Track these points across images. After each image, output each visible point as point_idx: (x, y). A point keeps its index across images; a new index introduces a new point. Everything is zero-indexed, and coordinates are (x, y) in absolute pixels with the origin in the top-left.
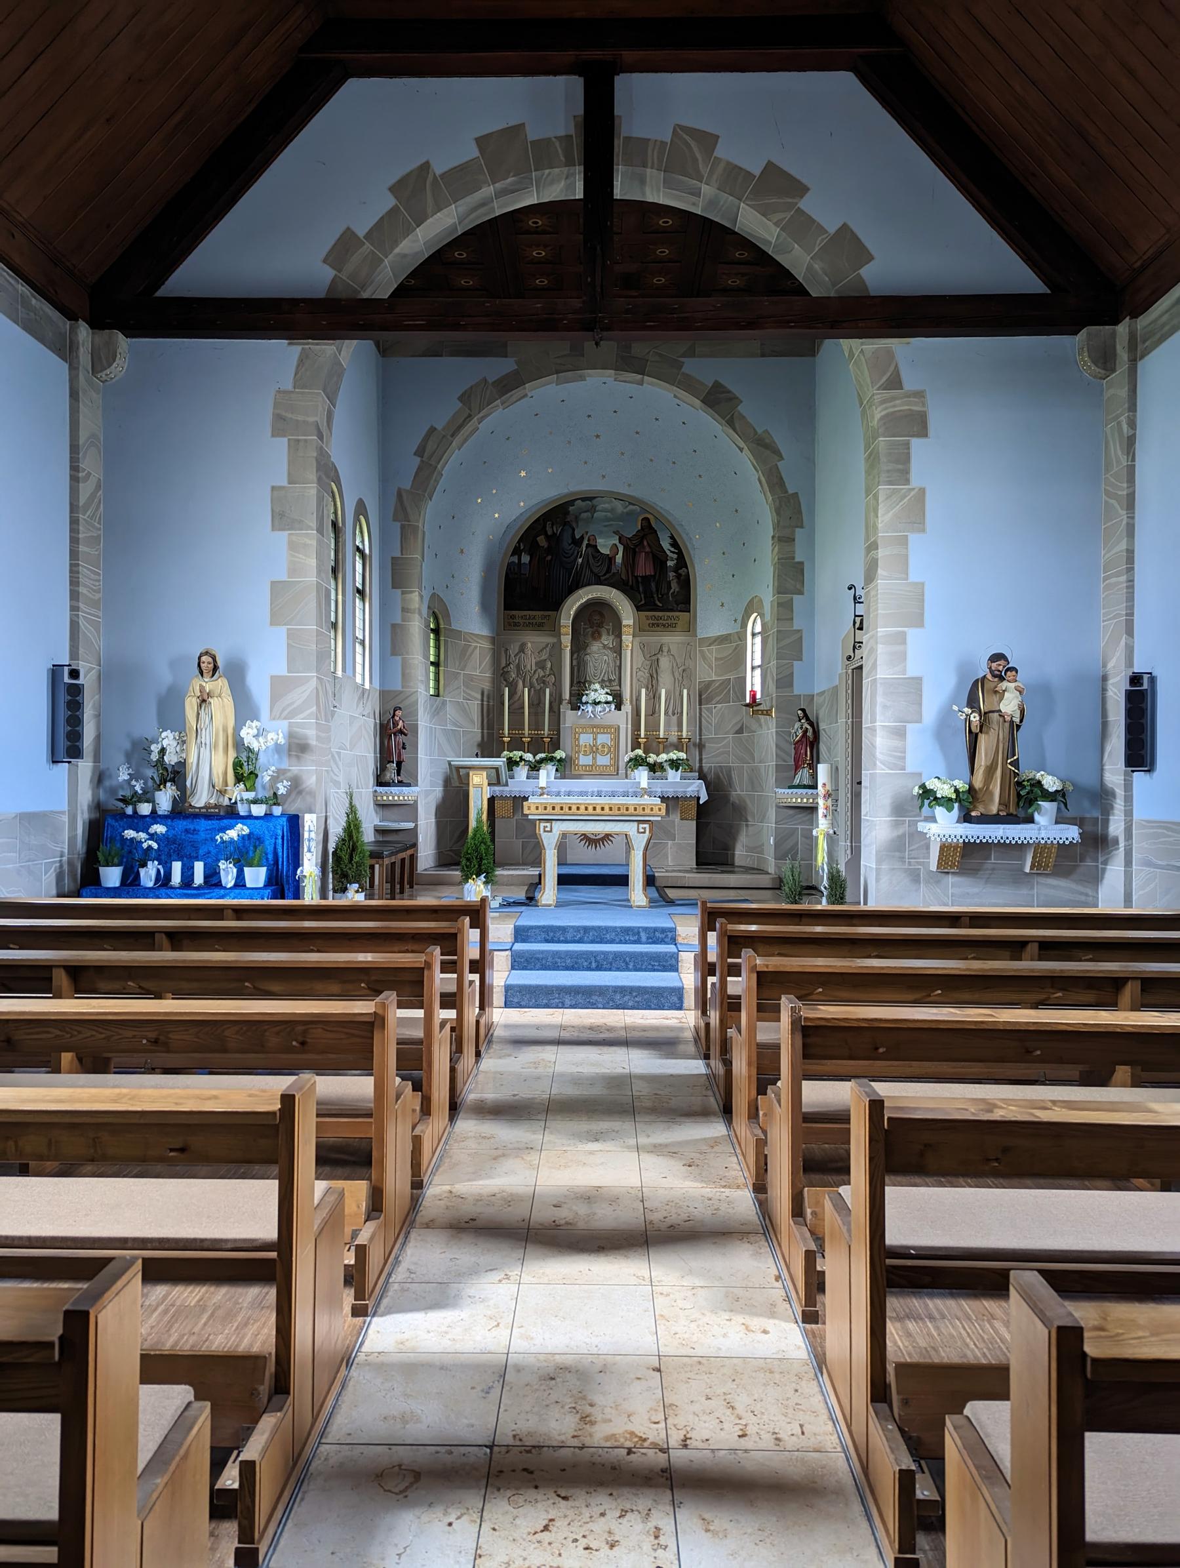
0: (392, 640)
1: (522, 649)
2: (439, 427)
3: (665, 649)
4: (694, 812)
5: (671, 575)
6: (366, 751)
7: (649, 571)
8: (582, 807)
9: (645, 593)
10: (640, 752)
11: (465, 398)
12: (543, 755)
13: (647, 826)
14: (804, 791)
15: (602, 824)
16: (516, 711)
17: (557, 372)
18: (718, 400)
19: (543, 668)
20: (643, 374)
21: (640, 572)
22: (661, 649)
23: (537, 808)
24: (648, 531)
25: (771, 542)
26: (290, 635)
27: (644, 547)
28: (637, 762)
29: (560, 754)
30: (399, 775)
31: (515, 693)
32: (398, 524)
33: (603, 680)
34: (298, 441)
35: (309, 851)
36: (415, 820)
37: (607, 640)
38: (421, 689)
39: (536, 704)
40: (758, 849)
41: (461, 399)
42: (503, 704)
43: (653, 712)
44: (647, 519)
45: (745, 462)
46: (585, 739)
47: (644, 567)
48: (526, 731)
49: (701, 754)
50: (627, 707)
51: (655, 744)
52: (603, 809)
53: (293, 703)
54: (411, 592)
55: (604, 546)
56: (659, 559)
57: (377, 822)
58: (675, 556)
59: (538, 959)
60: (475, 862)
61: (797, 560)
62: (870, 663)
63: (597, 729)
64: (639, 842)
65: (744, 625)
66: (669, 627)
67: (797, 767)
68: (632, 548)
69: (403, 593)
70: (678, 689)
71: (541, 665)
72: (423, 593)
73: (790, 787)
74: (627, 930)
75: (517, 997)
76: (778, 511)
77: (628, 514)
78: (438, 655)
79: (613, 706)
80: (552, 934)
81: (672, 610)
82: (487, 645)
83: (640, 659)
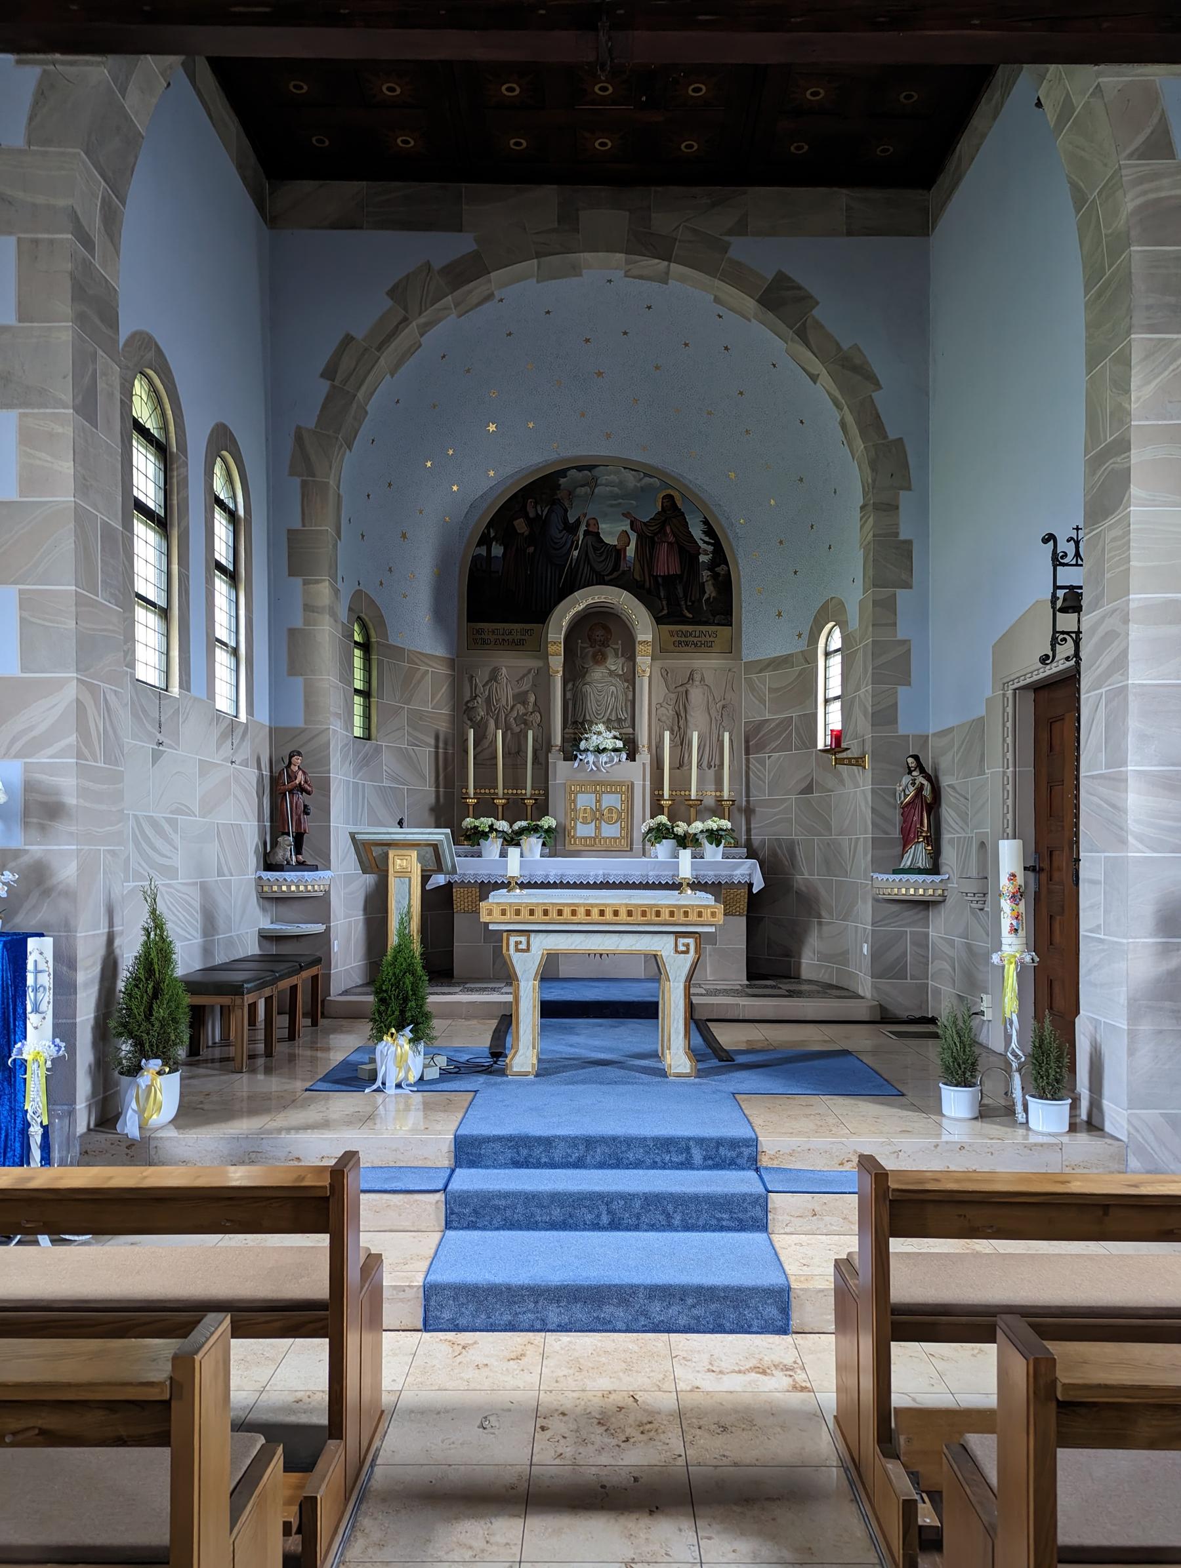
0: (289, 652)
1: (494, 676)
2: (359, 335)
3: (697, 677)
4: (743, 905)
5: (706, 574)
6: (242, 818)
8: (581, 911)
10: (663, 819)
11: (397, 293)
12: (524, 823)
13: (691, 941)
14: (920, 878)
15: (615, 937)
16: (486, 763)
17: (538, 255)
18: (782, 300)
19: (525, 703)
20: (670, 260)
22: (691, 678)
23: (504, 913)
24: (672, 513)
25: (857, 514)
26: (25, 602)
27: (665, 534)
28: (660, 833)
29: (548, 822)
30: (298, 851)
31: (484, 736)
32: (298, 480)
34: (36, 242)
35: (36, 1010)
36: (326, 919)
37: (614, 664)
38: (336, 727)
39: (514, 753)
40: (842, 957)
41: (391, 293)
42: (466, 752)
43: (680, 764)
44: (670, 497)
45: (820, 400)
46: (585, 801)
47: (666, 564)
49: (748, 823)
50: (644, 757)
52: (616, 913)
53: (31, 728)
54: (317, 582)
55: (611, 533)
56: (687, 552)
57: (266, 924)
58: (710, 548)
59: (497, 1208)
60: (394, 1005)
61: (902, 537)
62: (1105, 660)
63: (601, 786)
64: (678, 967)
65: (813, 640)
66: (701, 646)
67: (906, 842)
68: (648, 539)
69: (305, 583)
70: (715, 732)
71: (521, 698)
72: (340, 585)
73: (895, 872)
74: (666, 1144)
75: (452, 1308)
76: (874, 465)
77: (642, 489)
78: (368, 681)
79: (624, 756)
80: (525, 1151)
82: (443, 670)
83: (661, 690)
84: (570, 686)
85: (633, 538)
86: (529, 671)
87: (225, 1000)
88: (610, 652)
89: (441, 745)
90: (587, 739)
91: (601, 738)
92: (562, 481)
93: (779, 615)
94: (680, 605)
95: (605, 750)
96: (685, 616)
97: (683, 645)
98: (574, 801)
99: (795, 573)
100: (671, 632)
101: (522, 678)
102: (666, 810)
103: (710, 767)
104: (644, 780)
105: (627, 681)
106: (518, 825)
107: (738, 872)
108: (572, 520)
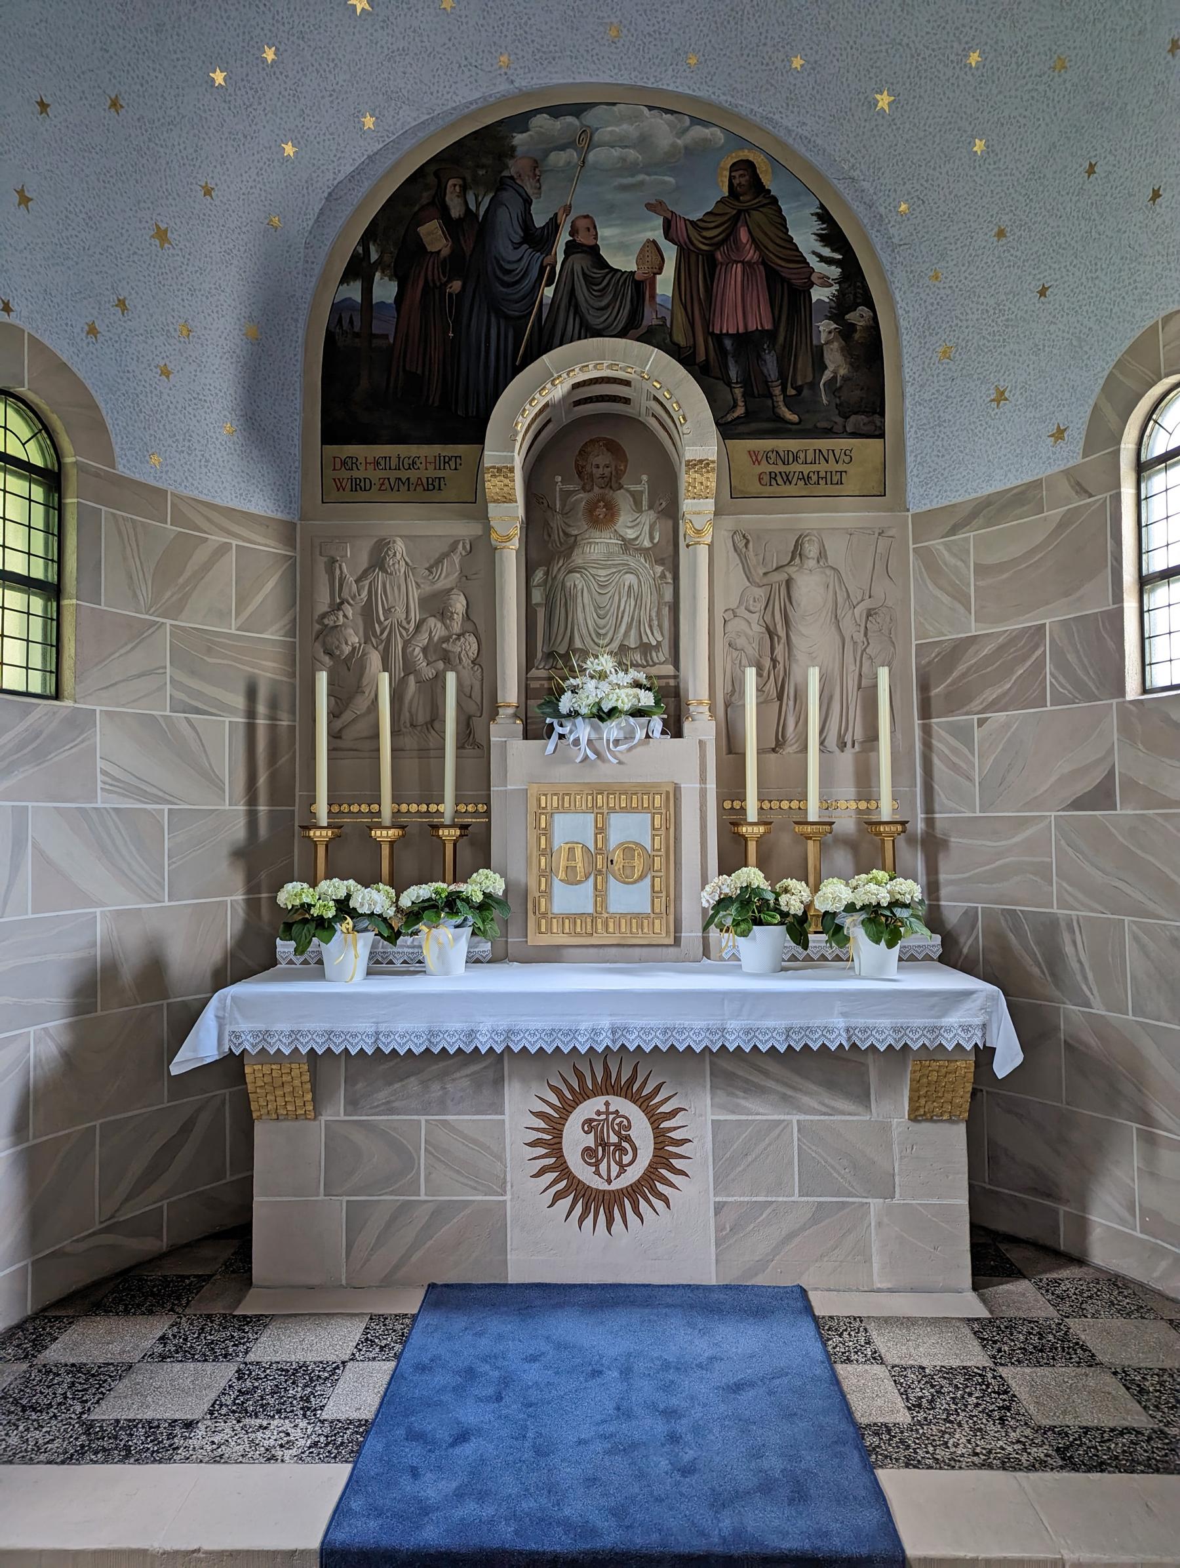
1: (379, 560)
3: (811, 550)
5: (824, 328)
7: (759, 318)
9: (746, 383)
10: (751, 875)
16: (353, 745)
19: (443, 614)
21: (730, 323)
22: (797, 552)
24: (750, 194)
27: (738, 247)
28: (750, 910)
29: (484, 883)
33: (623, 649)
37: (635, 524)
44: (748, 166)
46: (571, 828)
47: (742, 308)
48: (387, 807)
50: (702, 727)
51: (785, 840)
55: (622, 247)
56: (786, 285)
58: (834, 272)
63: (606, 798)
66: (824, 483)
68: (701, 262)
71: (436, 605)
77: (689, 151)
79: (657, 724)
81: (828, 433)
82: (267, 546)
83: (734, 580)
84: (539, 575)
85: (671, 254)
86: (453, 548)
87: (592, 756)
88: (623, 500)
91: (605, 686)
92: (519, 139)
93: (1000, 397)
95: (613, 712)
97: (780, 480)
98: (547, 832)
99: (1043, 292)
100: (755, 457)
101: (439, 561)
102: (752, 847)
103: (842, 746)
104: (703, 780)
105: (660, 562)
107: (952, 1020)
108: (539, 221)
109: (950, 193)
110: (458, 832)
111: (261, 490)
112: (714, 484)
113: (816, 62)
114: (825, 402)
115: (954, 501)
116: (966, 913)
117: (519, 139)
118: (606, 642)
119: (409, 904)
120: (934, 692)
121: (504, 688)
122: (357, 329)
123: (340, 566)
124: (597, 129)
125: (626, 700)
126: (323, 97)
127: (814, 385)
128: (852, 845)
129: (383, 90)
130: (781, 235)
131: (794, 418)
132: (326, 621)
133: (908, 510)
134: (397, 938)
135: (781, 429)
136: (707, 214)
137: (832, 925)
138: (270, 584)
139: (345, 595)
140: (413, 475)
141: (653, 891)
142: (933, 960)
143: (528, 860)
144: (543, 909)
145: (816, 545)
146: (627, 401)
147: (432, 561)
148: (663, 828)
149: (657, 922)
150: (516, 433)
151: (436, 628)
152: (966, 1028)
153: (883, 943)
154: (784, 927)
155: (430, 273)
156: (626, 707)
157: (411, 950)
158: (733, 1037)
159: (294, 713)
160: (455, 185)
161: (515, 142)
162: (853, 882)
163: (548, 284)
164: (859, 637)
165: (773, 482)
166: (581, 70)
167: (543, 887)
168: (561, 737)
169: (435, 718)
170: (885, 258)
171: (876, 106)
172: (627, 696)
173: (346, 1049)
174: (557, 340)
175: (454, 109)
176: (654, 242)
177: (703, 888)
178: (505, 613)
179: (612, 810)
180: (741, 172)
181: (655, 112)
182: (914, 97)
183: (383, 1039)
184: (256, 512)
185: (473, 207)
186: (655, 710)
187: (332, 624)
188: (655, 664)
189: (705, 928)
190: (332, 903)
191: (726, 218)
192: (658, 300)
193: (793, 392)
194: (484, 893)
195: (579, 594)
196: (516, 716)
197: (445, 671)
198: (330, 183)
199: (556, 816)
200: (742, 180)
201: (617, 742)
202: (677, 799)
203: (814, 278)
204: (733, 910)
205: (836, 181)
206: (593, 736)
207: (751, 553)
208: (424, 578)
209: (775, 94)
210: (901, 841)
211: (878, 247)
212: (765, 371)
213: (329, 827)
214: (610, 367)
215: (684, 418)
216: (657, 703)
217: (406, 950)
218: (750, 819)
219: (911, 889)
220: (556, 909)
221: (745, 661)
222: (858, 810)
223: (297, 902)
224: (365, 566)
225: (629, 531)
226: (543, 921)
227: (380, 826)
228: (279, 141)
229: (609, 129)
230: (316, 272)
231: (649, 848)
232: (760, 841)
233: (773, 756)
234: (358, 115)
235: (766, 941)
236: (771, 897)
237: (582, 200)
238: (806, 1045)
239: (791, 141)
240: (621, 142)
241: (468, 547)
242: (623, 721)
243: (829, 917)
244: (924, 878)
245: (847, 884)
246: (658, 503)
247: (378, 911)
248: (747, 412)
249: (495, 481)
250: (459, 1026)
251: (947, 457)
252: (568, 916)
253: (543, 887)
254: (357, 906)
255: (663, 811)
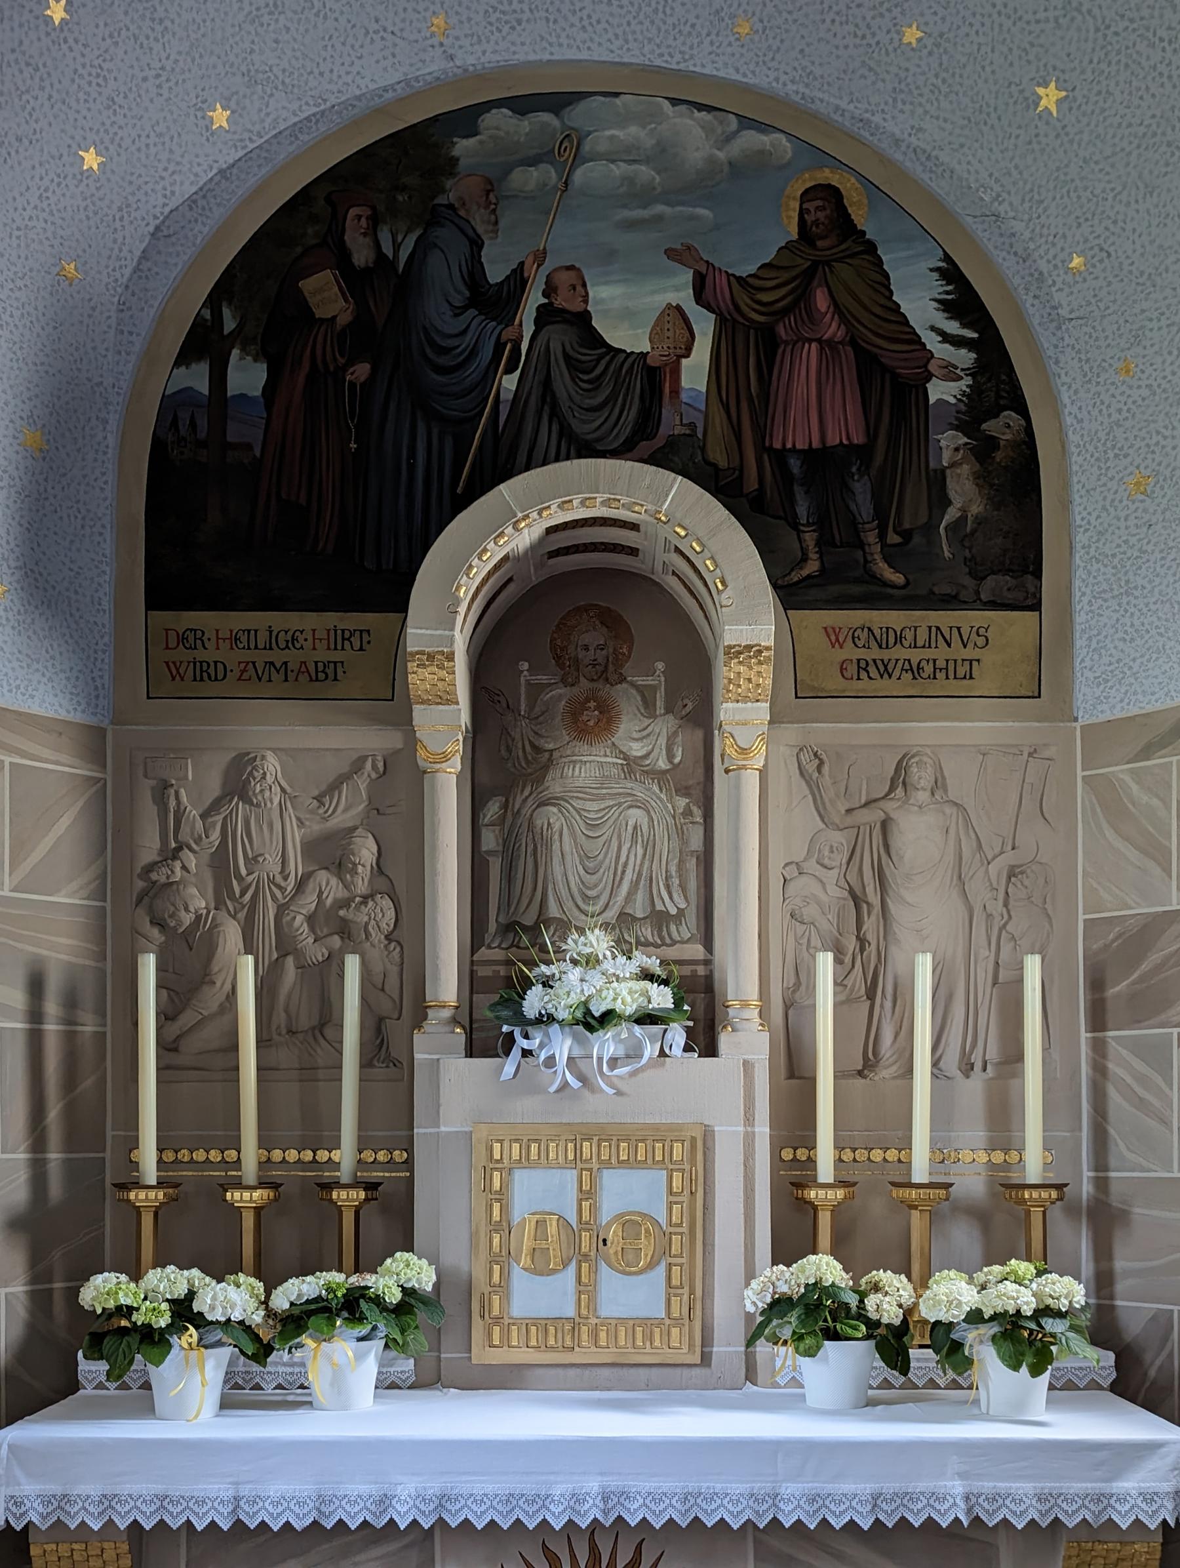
1: (239, 783)
3: (922, 776)
7: (844, 425)
9: (822, 523)
16: (195, 1060)
19: (341, 866)
22: (900, 779)
24: (835, 235)
28: (819, 1318)
33: (625, 919)
37: (645, 736)
39: (295, 1032)
43: (871, 1058)
44: (831, 195)
47: (816, 409)
50: (748, 1041)
51: (877, 1207)
55: (628, 315)
56: (886, 372)
58: (965, 358)
63: (599, 1146)
66: (942, 677)
68: (755, 328)
71: (329, 852)
77: (736, 169)
79: (677, 1035)
81: (950, 602)
82: (60, 764)
83: (799, 822)
84: (493, 809)
85: (704, 326)
86: (357, 766)
88: (626, 701)
89: (52, 1007)
90: (547, 983)
91: (596, 979)
92: (463, 147)
94: (861, 545)
95: (607, 1018)
96: (886, 584)
97: (874, 672)
98: (503, 1196)
101: (334, 787)
102: (825, 1220)
103: (967, 1068)
104: (749, 1119)
105: (684, 791)
106: (296, 1290)
107: (1129, 1485)
108: (496, 273)
109: (1152, 242)
110: (362, 1195)
111: (50, 680)
112: (769, 682)
113: (941, 35)
114: (947, 554)
115: (1149, 709)
116: (1154, 1318)
117: (463, 147)
118: (598, 908)
119: (287, 1306)
120: (1111, 992)
121: (436, 978)
122: (202, 435)
123: (177, 793)
124: (589, 133)
125: (629, 999)
126: (145, 79)
127: (930, 528)
128: (981, 1216)
129: (244, 68)
130: (883, 301)
131: (899, 579)
132: (154, 876)
133: (1076, 719)
134: (267, 1355)
135: (878, 596)
136: (763, 266)
137: (947, 1343)
138: (65, 822)
139: (185, 835)
140: (293, 657)
141: (671, 1192)
142: (1101, 1388)
143: (473, 1237)
144: (496, 1312)
145: (930, 770)
146: (633, 552)
147: (324, 787)
148: (686, 1192)
149: (675, 1332)
150: (457, 601)
151: (330, 887)
152: (1149, 1497)
153: (1024, 1369)
154: (871, 1344)
155: (319, 347)
156: (629, 1010)
157: (289, 1370)
158: (791, 1507)
159: (104, 1016)
160: (359, 217)
161: (456, 151)
162: (980, 1277)
163: (509, 370)
164: (997, 908)
165: (863, 675)
166: (565, 41)
167: (496, 1278)
168: (526, 1053)
169: (327, 1019)
170: (1046, 340)
171: (1037, 105)
172: (631, 992)
173: (188, 1522)
174: (522, 458)
175: (358, 98)
176: (679, 308)
177: (747, 1284)
178: (439, 866)
179: (607, 1164)
180: (819, 203)
181: (683, 108)
182: (1099, 93)
183: (246, 1508)
184: (41, 712)
185: (388, 250)
186: (674, 1015)
187: (163, 879)
188: (674, 943)
189: (750, 1342)
190: (165, 1306)
191: (794, 273)
192: (684, 397)
193: (897, 539)
194: (404, 1290)
195: (556, 837)
196: (454, 1021)
197: (342, 952)
198: (158, 210)
199: (518, 1175)
200: (819, 214)
201: (614, 1062)
202: (708, 1151)
203: (932, 367)
204: (793, 1318)
205: (969, 219)
206: (576, 1052)
207: (826, 780)
208: (312, 812)
209: (874, 83)
210: (1056, 1212)
211: (1036, 322)
212: (853, 507)
213: (160, 1184)
214: (606, 503)
215: (723, 583)
216: (678, 1003)
217: (281, 1369)
218: (822, 1179)
219: (1069, 1291)
220: (516, 1311)
221: (816, 942)
222: (990, 1164)
223: (111, 1304)
224: (217, 792)
225: (635, 746)
226: (497, 1329)
227: (239, 1185)
228: (74, 146)
229: (608, 133)
230: (137, 348)
231: (663, 1221)
232: (837, 1210)
233: (860, 1082)
234: (202, 107)
235: (842, 1363)
236: (852, 1300)
237: (565, 241)
238: (903, 1519)
239: (898, 156)
240: (627, 154)
241: (380, 765)
242: (624, 1030)
243: (941, 1330)
244: (1091, 1266)
245: (971, 1281)
246: (680, 703)
247: (236, 1316)
248: (823, 570)
249: (424, 673)
250: (364, 1489)
251: (1139, 642)
252: (535, 1321)
253: (496, 1278)
254: (205, 1309)
255: (687, 1167)
